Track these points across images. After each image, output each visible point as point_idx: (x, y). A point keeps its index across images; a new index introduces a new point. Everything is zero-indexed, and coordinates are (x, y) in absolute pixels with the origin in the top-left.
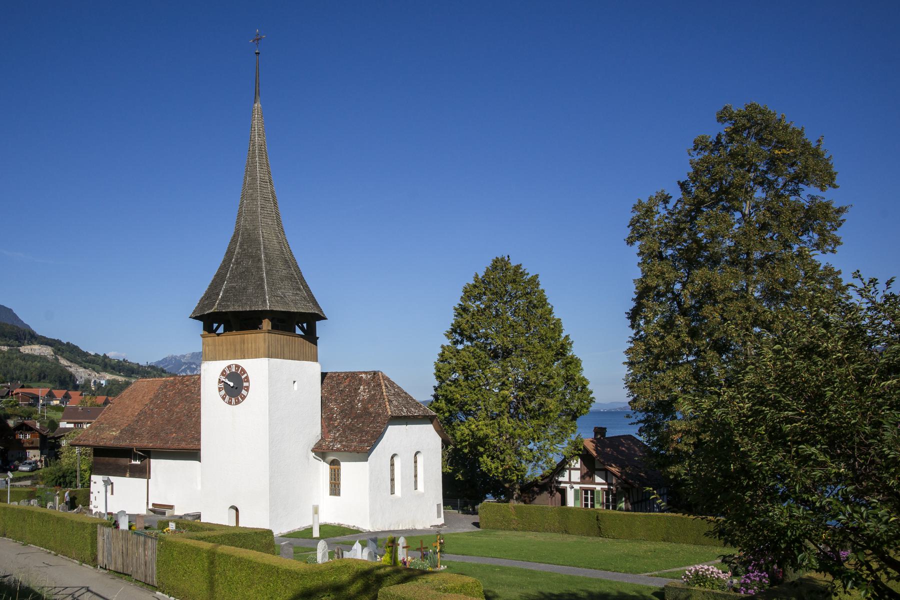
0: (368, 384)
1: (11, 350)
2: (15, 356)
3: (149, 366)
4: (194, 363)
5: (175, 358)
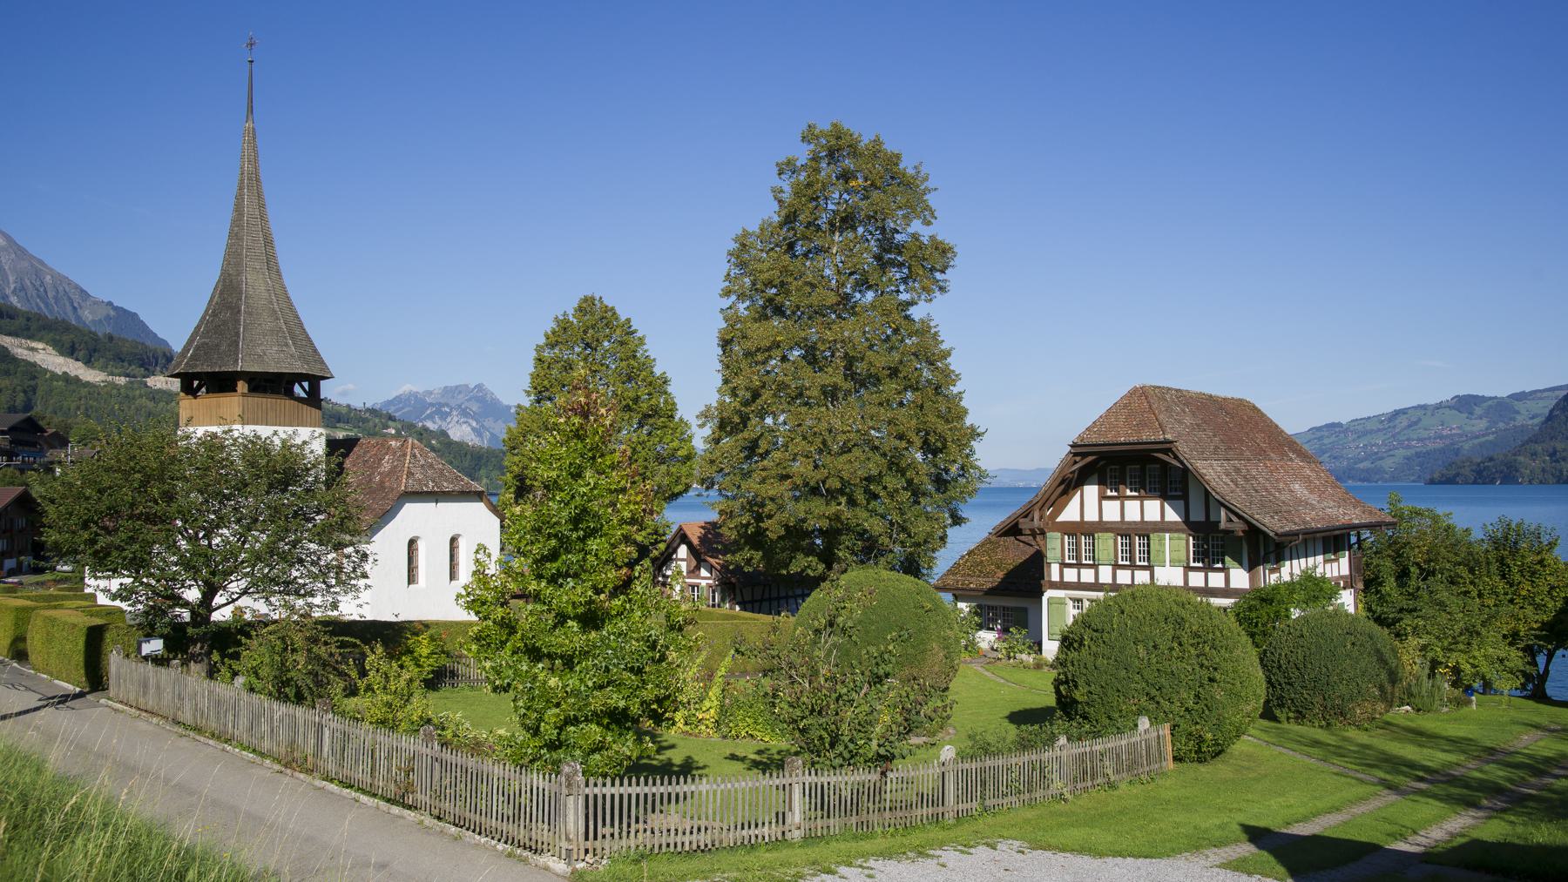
0: (394, 454)
1: (131, 383)
2: (138, 392)
3: (368, 410)
4: (447, 405)
5: (415, 395)
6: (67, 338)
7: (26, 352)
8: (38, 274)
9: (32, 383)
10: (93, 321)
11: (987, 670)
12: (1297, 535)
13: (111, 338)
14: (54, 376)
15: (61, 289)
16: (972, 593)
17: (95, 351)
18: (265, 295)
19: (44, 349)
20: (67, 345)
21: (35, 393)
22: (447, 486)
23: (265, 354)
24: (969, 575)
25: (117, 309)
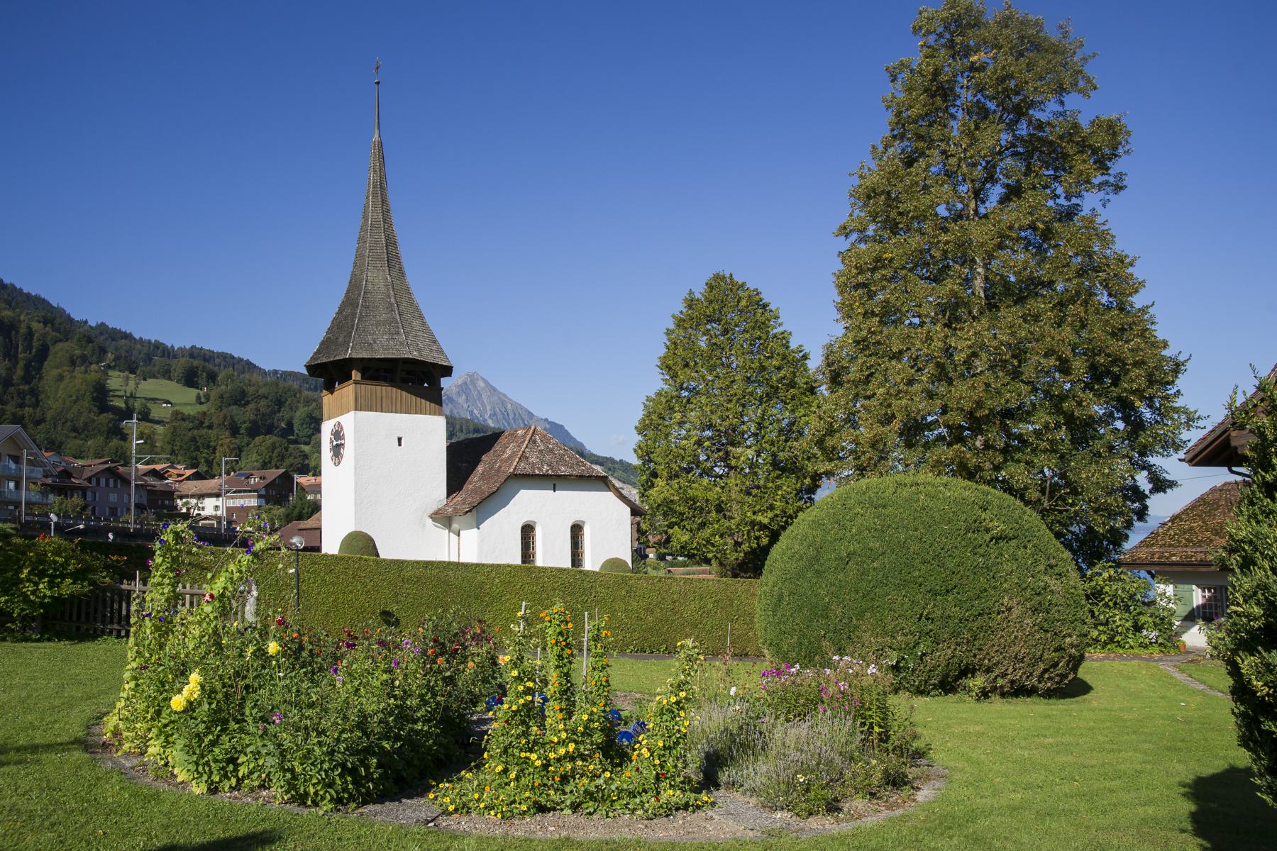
8: (503, 403)
11: (1182, 671)
15: (517, 413)
16: (1175, 569)
18: (383, 289)
22: (563, 470)
23: (375, 342)
24: (1170, 545)
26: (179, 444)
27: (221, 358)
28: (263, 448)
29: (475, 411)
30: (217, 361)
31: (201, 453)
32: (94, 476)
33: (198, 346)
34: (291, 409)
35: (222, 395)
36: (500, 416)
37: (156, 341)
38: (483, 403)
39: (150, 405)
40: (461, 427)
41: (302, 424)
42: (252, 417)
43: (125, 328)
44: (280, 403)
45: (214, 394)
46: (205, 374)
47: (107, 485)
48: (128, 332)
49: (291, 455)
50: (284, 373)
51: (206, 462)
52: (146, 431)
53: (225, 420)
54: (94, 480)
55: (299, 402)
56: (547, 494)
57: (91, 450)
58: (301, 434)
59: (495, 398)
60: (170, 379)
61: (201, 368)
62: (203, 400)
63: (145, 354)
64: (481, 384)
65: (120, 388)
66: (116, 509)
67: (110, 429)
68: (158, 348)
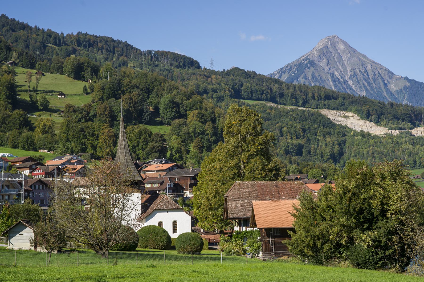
2: (403, 140)
6: (364, 108)
7: (343, 119)
8: (363, 64)
9: (343, 138)
10: (397, 91)
12: (241, 218)
13: (392, 105)
14: (356, 133)
15: (377, 73)
17: (382, 114)
18: (124, 161)
19: (353, 117)
20: (365, 113)
21: (345, 145)
25: (410, 81)
26: (72, 134)
27: (103, 42)
28: (133, 135)
29: (336, 73)
30: (100, 45)
31: (88, 140)
32: (33, 184)
33: (84, 32)
34: (157, 95)
35: (103, 87)
36: (360, 77)
37: (48, 30)
38: (343, 65)
39: (48, 97)
40: (313, 94)
41: (166, 108)
42: (126, 106)
43: (21, 19)
44: (149, 91)
45: (97, 86)
46: (89, 69)
47: (39, 188)
48: (25, 23)
49: (153, 140)
50: (157, 52)
51: (91, 146)
52: (47, 124)
53: (105, 111)
54: (33, 186)
55: (163, 90)
56: (166, 214)
57: (9, 140)
58: (165, 117)
59: (355, 59)
60: (62, 73)
61: (86, 64)
62: (89, 91)
63: (40, 42)
64: (341, 47)
65: (24, 83)
66: (43, 200)
67: (21, 122)
68: (50, 36)
